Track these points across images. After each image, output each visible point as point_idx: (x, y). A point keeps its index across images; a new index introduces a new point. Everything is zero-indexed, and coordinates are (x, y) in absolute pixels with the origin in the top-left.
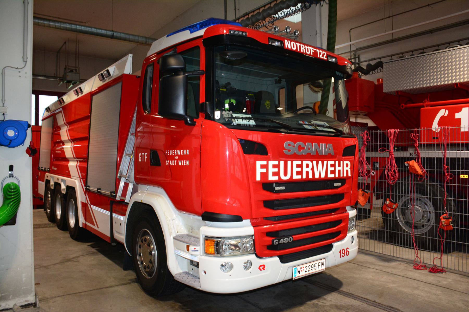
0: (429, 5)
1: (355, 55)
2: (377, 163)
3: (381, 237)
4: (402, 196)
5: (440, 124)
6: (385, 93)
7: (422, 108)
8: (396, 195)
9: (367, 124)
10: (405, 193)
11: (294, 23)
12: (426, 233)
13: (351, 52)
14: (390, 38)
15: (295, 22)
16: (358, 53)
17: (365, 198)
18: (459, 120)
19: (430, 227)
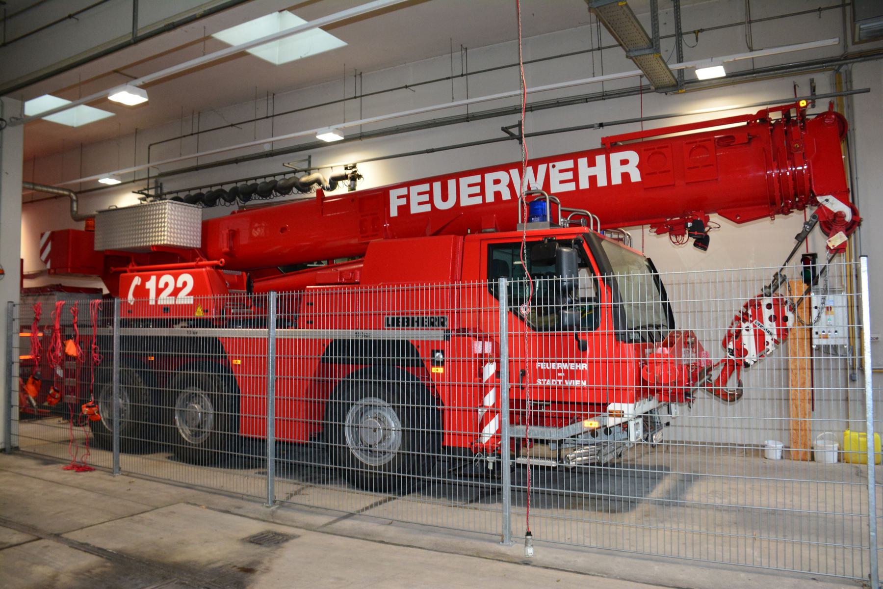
0: (406, 87)
1: (156, 182)
2: (438, 351)
3: (315, 478)
4: (353, 404)
5: (134, 295)
6: (98, 252)
7: (122, 275)
8: (335, 403)
9: (101, 290)
10: (357, 400)
11: (73, 127)
12: (380, 467)
13: (149, 178)
14: (462, 112)
15: (75, 125)
16: (161, 180)
17: (36, 387)
18: (148, 290)
19: (392, 456)
